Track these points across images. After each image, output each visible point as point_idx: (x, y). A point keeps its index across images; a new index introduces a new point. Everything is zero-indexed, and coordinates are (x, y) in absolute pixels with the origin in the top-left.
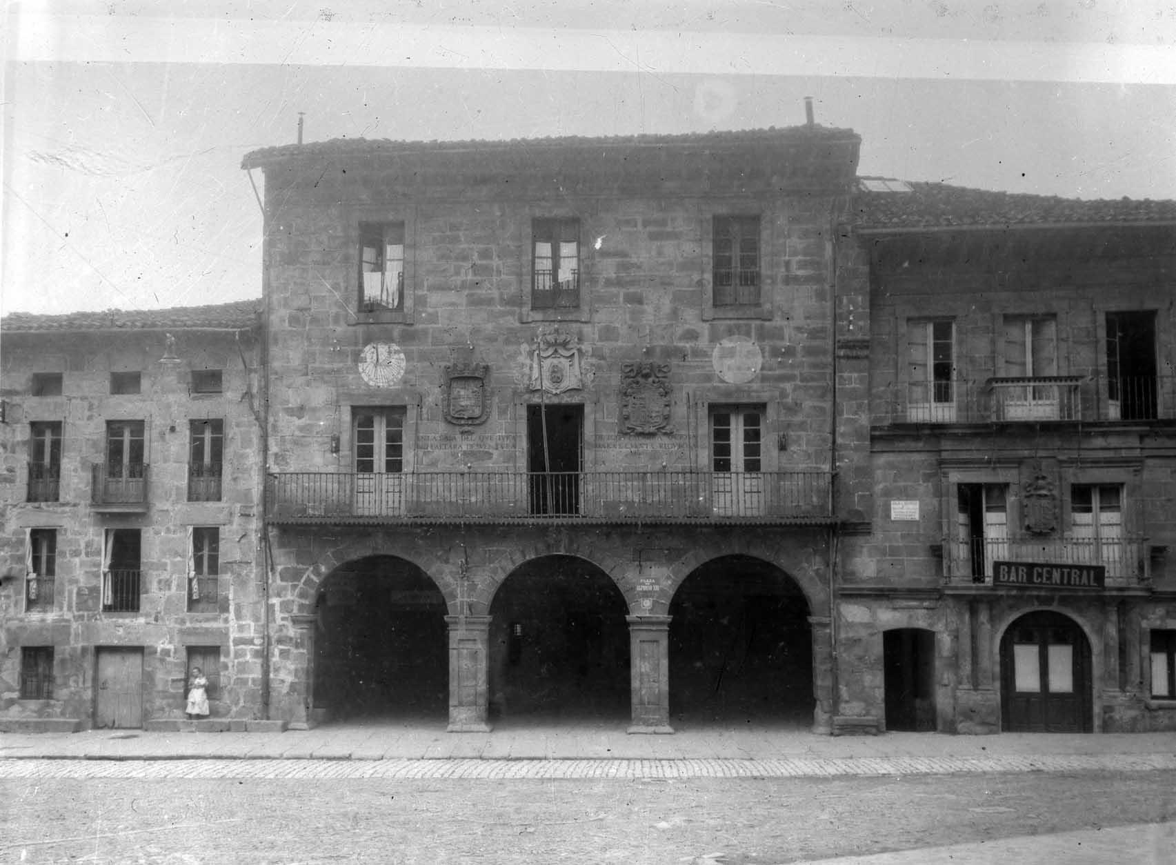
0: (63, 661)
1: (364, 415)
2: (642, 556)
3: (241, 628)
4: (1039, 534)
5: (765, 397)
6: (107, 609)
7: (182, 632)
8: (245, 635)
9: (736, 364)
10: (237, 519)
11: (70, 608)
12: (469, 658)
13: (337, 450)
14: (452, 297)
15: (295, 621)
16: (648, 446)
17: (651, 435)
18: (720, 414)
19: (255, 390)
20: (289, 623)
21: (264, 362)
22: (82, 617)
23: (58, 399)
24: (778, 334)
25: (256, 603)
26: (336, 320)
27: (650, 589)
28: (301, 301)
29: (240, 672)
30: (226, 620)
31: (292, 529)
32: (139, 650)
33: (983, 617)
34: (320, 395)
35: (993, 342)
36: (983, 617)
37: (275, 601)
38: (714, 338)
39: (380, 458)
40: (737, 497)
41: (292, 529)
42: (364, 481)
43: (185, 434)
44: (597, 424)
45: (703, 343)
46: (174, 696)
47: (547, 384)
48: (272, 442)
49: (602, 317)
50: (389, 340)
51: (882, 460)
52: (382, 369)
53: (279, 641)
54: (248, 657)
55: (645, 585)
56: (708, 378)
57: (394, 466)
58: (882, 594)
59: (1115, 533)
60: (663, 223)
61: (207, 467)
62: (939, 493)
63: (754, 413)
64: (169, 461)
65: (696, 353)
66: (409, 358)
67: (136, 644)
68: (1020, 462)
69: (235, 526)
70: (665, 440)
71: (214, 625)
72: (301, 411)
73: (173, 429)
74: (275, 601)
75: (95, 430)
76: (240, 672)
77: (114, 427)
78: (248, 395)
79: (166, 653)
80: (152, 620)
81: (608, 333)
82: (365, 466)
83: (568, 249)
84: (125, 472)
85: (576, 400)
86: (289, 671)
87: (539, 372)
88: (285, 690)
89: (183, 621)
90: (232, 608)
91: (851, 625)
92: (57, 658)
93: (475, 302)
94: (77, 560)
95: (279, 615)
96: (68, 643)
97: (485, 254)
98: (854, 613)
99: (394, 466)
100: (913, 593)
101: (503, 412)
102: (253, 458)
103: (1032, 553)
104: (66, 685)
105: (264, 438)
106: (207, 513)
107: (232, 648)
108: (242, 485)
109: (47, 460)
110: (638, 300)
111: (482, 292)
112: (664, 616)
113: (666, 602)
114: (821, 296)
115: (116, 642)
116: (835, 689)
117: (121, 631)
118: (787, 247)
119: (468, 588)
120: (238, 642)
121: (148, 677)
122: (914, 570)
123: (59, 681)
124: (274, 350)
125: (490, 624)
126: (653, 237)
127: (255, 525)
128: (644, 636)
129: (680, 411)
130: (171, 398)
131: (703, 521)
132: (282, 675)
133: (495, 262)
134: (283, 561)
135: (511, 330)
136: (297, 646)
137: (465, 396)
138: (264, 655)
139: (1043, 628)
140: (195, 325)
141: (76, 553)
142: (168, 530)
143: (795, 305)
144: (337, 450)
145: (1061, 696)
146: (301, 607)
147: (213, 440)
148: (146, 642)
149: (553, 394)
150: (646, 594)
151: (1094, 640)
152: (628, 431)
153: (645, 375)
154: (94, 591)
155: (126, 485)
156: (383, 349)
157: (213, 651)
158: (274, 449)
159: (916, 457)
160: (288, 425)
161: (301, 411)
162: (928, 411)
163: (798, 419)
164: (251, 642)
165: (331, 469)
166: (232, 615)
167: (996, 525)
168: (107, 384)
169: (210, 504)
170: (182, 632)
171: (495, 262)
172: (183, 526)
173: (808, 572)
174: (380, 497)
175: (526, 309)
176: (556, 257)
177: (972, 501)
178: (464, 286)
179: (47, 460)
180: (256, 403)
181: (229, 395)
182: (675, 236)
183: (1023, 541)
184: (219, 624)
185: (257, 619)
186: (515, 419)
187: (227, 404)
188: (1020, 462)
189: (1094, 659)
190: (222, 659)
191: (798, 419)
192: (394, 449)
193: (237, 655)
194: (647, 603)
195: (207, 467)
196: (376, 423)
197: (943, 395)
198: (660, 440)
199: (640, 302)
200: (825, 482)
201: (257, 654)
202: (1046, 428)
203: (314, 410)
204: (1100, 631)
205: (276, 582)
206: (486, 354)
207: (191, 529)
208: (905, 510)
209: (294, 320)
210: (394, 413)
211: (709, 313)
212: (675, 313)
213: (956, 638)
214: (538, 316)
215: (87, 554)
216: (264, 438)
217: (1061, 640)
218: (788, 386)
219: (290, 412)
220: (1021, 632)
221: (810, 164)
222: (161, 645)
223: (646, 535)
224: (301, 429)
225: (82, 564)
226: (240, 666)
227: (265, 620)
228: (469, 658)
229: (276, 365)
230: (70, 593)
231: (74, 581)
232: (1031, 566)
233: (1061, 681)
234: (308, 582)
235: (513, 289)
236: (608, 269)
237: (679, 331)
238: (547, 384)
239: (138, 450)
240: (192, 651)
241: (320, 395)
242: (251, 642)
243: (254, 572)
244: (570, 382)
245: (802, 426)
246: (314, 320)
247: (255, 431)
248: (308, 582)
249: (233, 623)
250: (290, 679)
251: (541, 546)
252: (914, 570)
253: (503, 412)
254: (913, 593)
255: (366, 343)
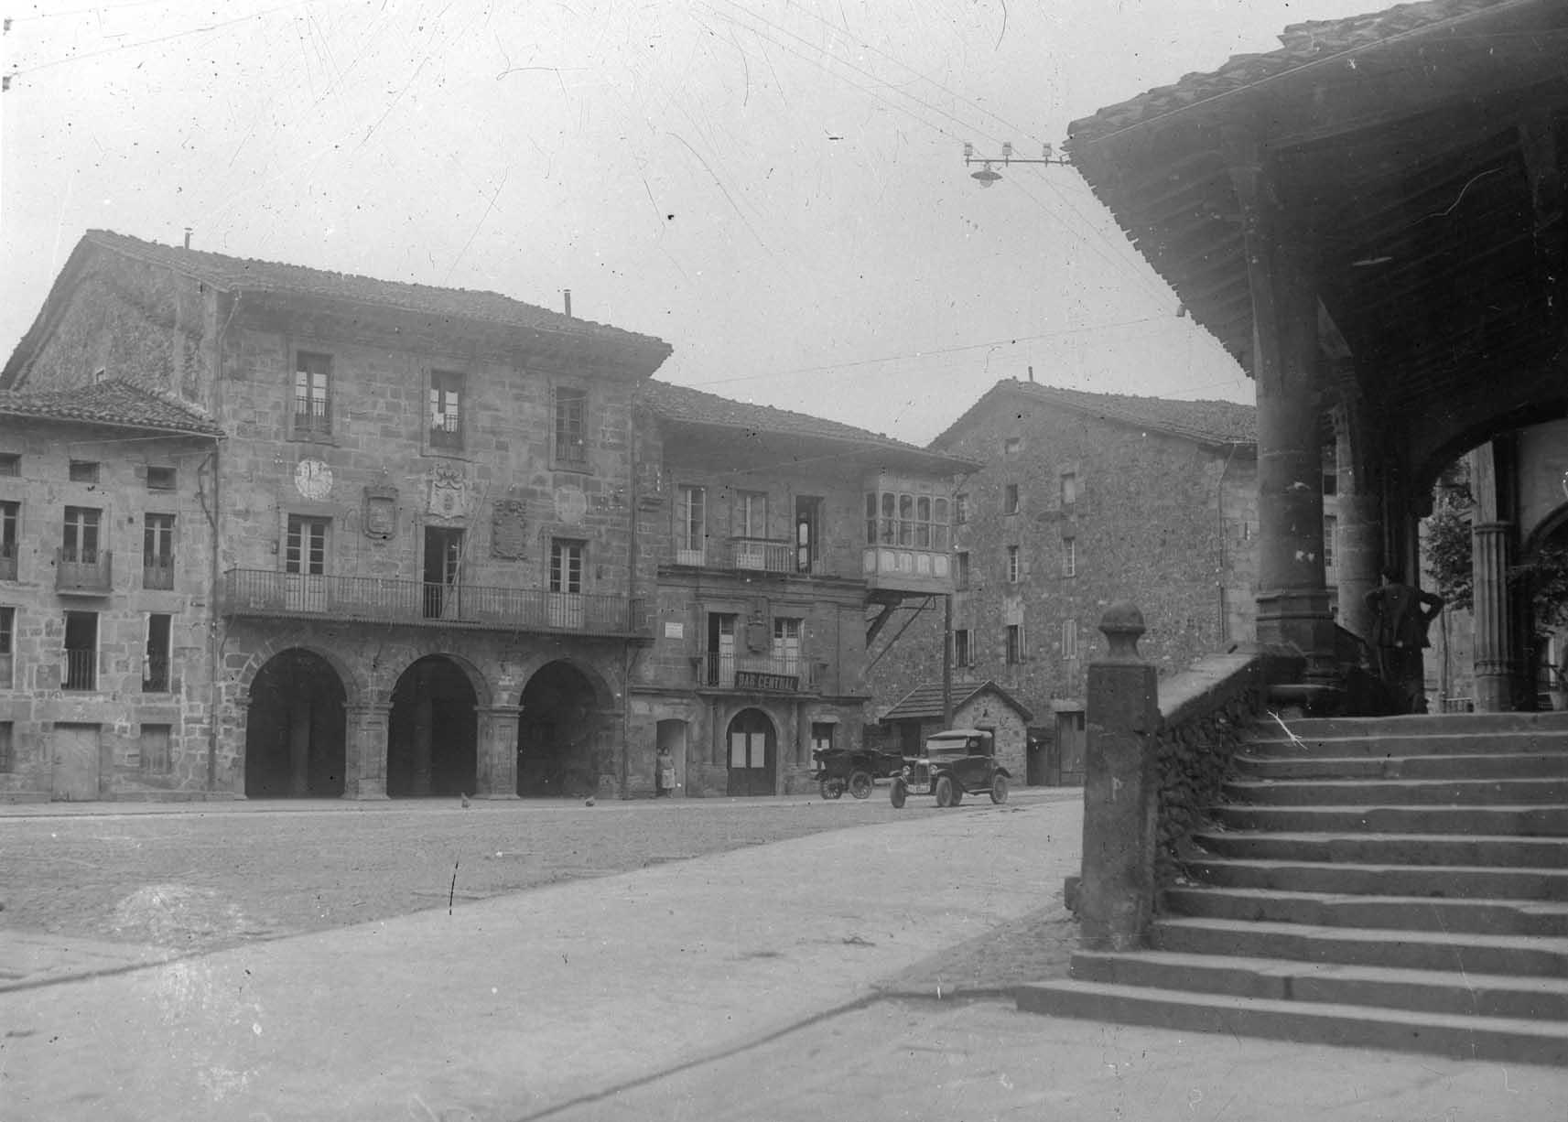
0: (24, 737)
1: (295, 522)
2: (503, 658)
3: (191, 709)
4: (755, 652)
5: (587, 536)
6: (65, 687)
7: (140, 711)
8: (196, 715)
9: (570, 508)
10: (189, 608)
11: (30, 685)
12: (368, 739)
13: (276, 552)
14: (371, 427)
15: (238, 703)
16: (510, 567)
17: (514, 559)
18: (557, 544)
19: (206, 491)
20: (232, 705)
21: (215, 467)
22: (42, 695)
23: (14, 480)
24: (597, 486)
25: (204, 687)
26: (277, 436)
27: (506, 683)
28: (245, 415)
29: (190, 748)
30: (178, 701)
31: (241, 622)
32: (96, 727)
33: (722, 711)
34: (262, 501)
35: (731, 509)
36: (722, 711)
37: (222, 684)
38: (556, 484)
39: (305, 561)
40: (565, 614)
41: (241, 622)
42: (293, 581)
43: (139, 528)
44: (473, 548)
45: (549, 488)
46: (131, 770)
47: (441, 510)
48: (221, 539)
49: (480, 458)
50: (319, 458)
51: (661, 590)
52: (312, 483)
53: (224, 721)
54: (197, 735)
55: (505, 681)
56: (552, 516)
57: (316, 569)
58: (659, 694)
59: (793, 653)
60: (523, 388)
61: (159, 559)
62: (696, 618)
63: (577, 546)
64: (122, 545)
65: (543, 494)
66: (335, 475)
67: (94, 721)
68: (746, 599)
69: (187, 615)
70: (522, 564)
71: (166, 705)
72: (246, 514)
73: (131, 520)
74: (222, 684)
75: (56, 514)
76: (190, 748)
77: (71, 512)
78: (201, 494)
79: (124, 730)
80: (109, 699)
81: (484, 472)
82: (293, 568)
83: (319, 379)
84: (79, 557)
85: (461, 525)
86: (231, 749)
87: (446, 503)
88: (228, 764)
89: (139, 701)
90: (183, 690)
91: (637, 716)
92: (16, 732)
93: (387, 433)
94: (38, 639)
95: (224, 698)
96: (28, 718)
97: (395, 395)
98: (639, 707)
99: (316, 569)
100: (680, 693)
101: (407, 530)
102: (203, 553)
103: (750, 665)
104: (27, 759)
105: (215, 535)
106: (162, 601)
107: (183, 726)
108: (195, 578)
109: (157, 551)
110: (502, 447)
111: (392, 426)
112: (516, 706)
113: (518, 695)
114: (625, 462)
115: (75, 719)
116: (624, 766)
117: (80, 708)
118: (607, 419)
119: (372, 678)
120: (188, 721)
121: (105, 752)
122: (677, 677)
123: (19, 755)
124: (224, 457)
125: (391, 710)
126: (518, 398)
127: (205, 614)
128: (503, 722)
129: (532, 541)
130: (129, 490)
131: (277, 613)
132: (225, 751)
133: (403, 402)
134: (232, 649)
135: (415, 462)
136: (238, 725)
137: (381, 513)
138: (211, 735)
139: (752, 721)
140: (190, 429)
141: (36, 632)
142: (126, 615)
143: (609, 467)
144: (276, 552)
145: (758, 769)
146: (243, 690)
147: (87, 530)
148: (105, 720)
149: (445, 519)
150: (505, 689)
151: (781, 731)
152: (498, 555)
153: (510, 510)
154: (54, 670)
155: (78, 568)
156: (315, 466)
157: (165, 729)
158: (223, 546)
159: (682, 590)
160: (234, 527)
161: (246, 514)
162: (687, 558)
163: (609, 555)
164: (200, 721)
165: (272, 568)
166: (183, 696)
167: (727, 643)
168: (67, 470)
169: (164, 593)
170: (140, 711)
171: (403, 402)
172: (141, 612)
173: (610, 672)
174: (305, 596)
175: (426, 445)
176: (310, 386)
177: (717, 623)
178: (380, 418)
179: (157, 551)
180: (208, 502)
181: (182, 494)
182: (530, 399)
183: (747, 657)
184: (172, 704)
185: (205, 700)
186: (416, 536)
187: (181, 501)
188: (746, 599)
189: (779, 743)
190: (174, 736)
191: (609, 555)
192: (317, 556)
193: (189, 732)
194: (505, 696)
195: (159, 559)
196: (309, 528)
197: (695, 547)
198: (520, 564)
199: (506, 449)
200: (624, 605)
201: (204, 732)
202: (754, 574)
203: (257, 514)
204: (786, 723)
205: (222, 666)
206: (400, 480)
207: (148, 616)
208: (674, 630)
209: (241, 430)
210: (320, 524)
211: (553, 465)
212: (530, 463)
213: (702, 727)
214: (434, 451)
215: (48, 634)
216: (215, 535)
217: (759, 730)
218: (603, 528)
219: (237, 514)
220: (737, 726)
221: (627, 359)
222: (120, 722)
223: (510, 640)
224: (247, 530)
225: (42, 644)
226: (188, 742)
227: (210, 699)
228: (368, 739)
229: (226, 470)
230: (31, 670)
231: (34, 660)
232: (757, 675)
233: (758, 761)
234: (250, 668)
235: (416, 427)
236: (484, 419)
237: (532, 477)
238: (441, 510)
239: (91, 536)
240: (147, 728)
241: (262, 501)
242: (200, 721)
243: (203, 658)
244: (456, 511)
245: (610, 561)
246: (258, 433)
247: (207, 527)
248: (250, 668)
249: (184, 703)
250: (232, 755)
251: (432, 645)
252: (677, 677)
253: (407, 530)
254: (680, 693)
255: (301, 459)
